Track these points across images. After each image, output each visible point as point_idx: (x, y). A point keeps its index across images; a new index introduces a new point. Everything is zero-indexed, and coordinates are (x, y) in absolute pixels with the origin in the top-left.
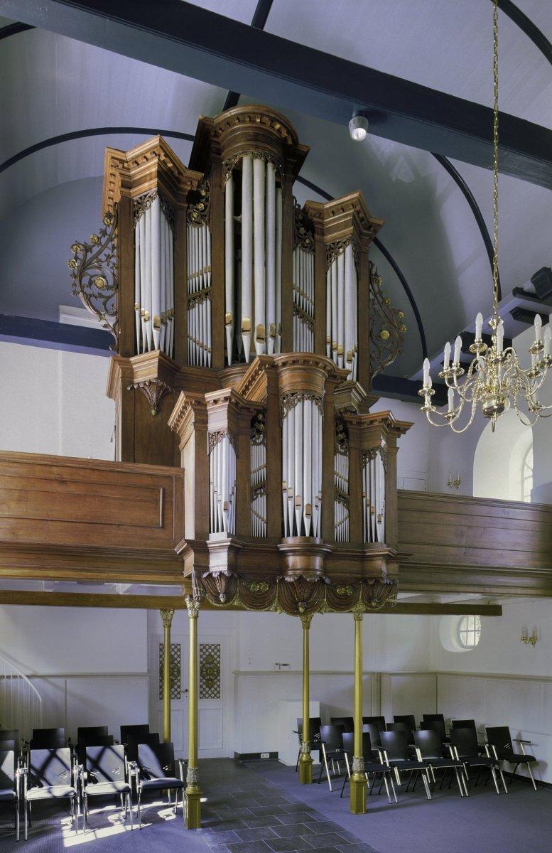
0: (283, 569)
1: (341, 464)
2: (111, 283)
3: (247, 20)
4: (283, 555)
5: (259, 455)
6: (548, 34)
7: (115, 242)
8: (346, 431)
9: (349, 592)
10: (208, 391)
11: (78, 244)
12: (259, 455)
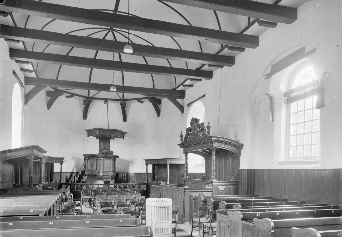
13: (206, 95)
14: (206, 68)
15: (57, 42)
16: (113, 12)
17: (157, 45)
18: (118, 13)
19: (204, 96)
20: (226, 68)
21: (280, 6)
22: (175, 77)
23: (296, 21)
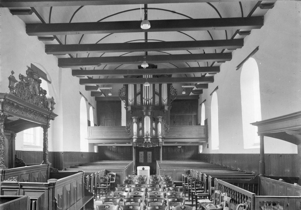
0: (144, 141)
1: (154, 124)
2: (124, 95)
3: (241, 17)
4: (144, 139)
5: (141, 125)
6: (102, 56)
7: (125, 88)
8: (155, 119)
9: (155, 144)
10: (132, 117)
11: (119, 90)
12: (141, 125)
13: (259, 48)
14: (226, 51)
15: (99, 31)
16: (144, 41)
17: (194, 17)
18: (148, 41)
19: (257, 49)
20: (227, 62)
21: (251, 17)
22: (194, 74)
23: (263, 26)
